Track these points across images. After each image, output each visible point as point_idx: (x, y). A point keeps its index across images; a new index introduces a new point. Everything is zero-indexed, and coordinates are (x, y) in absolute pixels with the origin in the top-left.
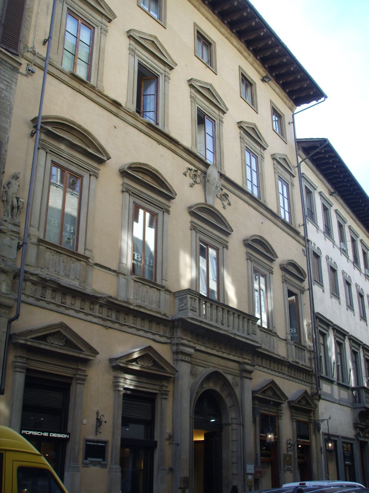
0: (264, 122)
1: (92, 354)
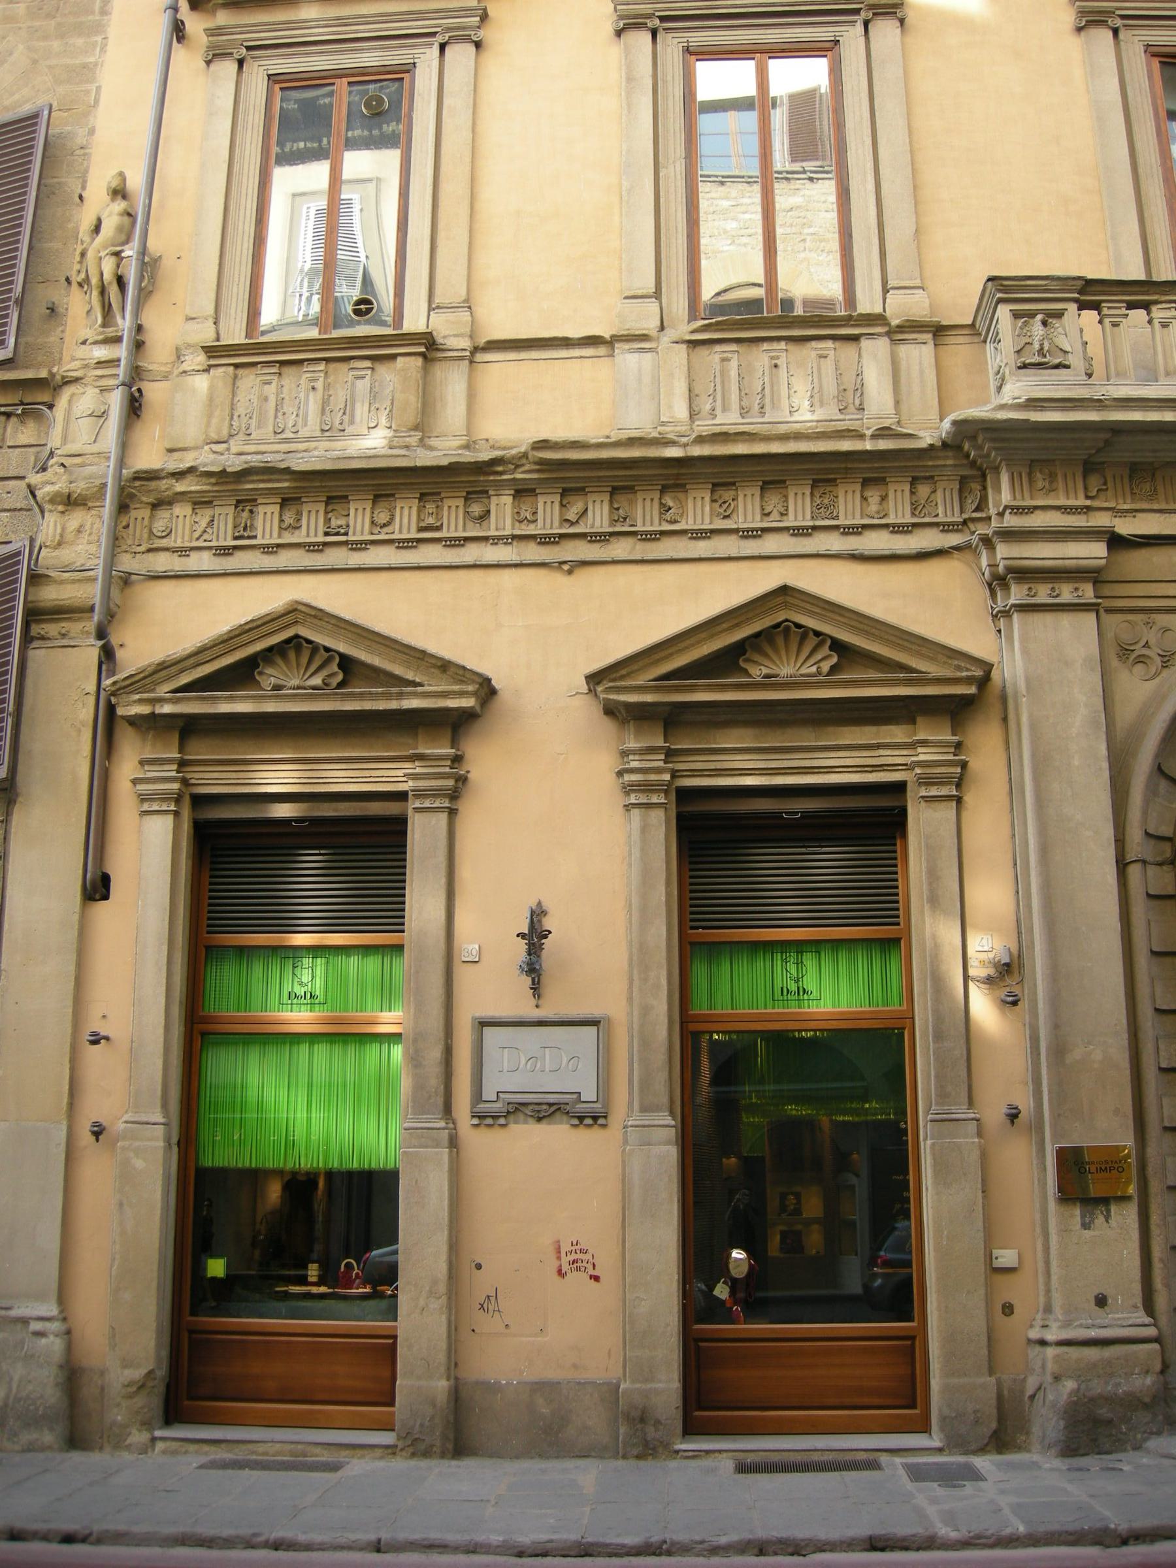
1: (456, 688)
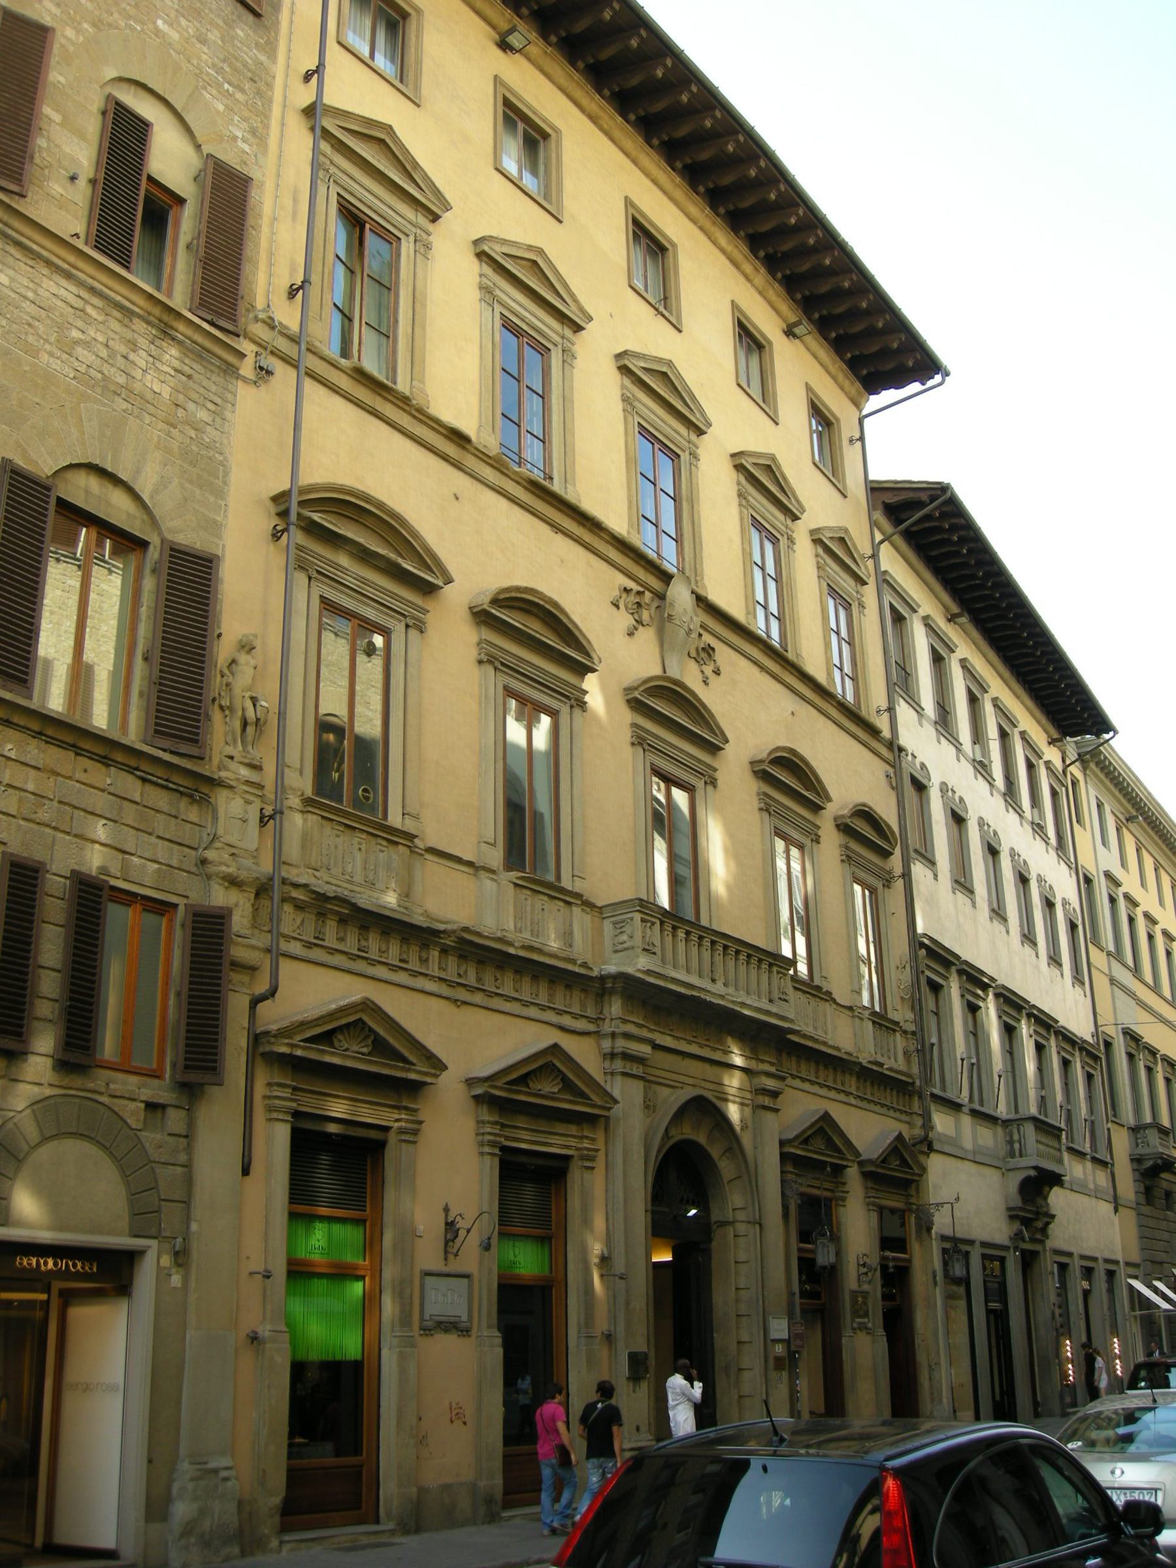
0: (790, 444)
1: (433, 1071)
